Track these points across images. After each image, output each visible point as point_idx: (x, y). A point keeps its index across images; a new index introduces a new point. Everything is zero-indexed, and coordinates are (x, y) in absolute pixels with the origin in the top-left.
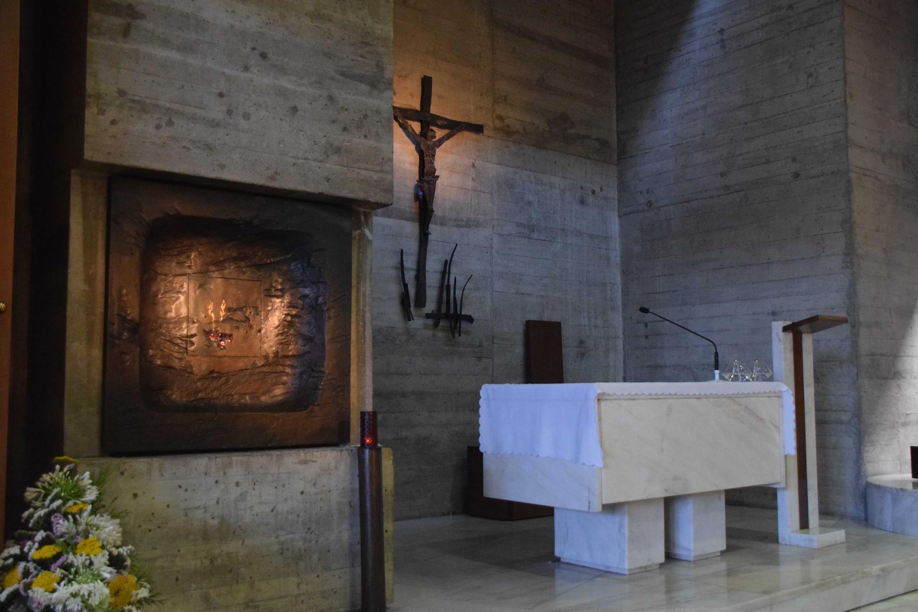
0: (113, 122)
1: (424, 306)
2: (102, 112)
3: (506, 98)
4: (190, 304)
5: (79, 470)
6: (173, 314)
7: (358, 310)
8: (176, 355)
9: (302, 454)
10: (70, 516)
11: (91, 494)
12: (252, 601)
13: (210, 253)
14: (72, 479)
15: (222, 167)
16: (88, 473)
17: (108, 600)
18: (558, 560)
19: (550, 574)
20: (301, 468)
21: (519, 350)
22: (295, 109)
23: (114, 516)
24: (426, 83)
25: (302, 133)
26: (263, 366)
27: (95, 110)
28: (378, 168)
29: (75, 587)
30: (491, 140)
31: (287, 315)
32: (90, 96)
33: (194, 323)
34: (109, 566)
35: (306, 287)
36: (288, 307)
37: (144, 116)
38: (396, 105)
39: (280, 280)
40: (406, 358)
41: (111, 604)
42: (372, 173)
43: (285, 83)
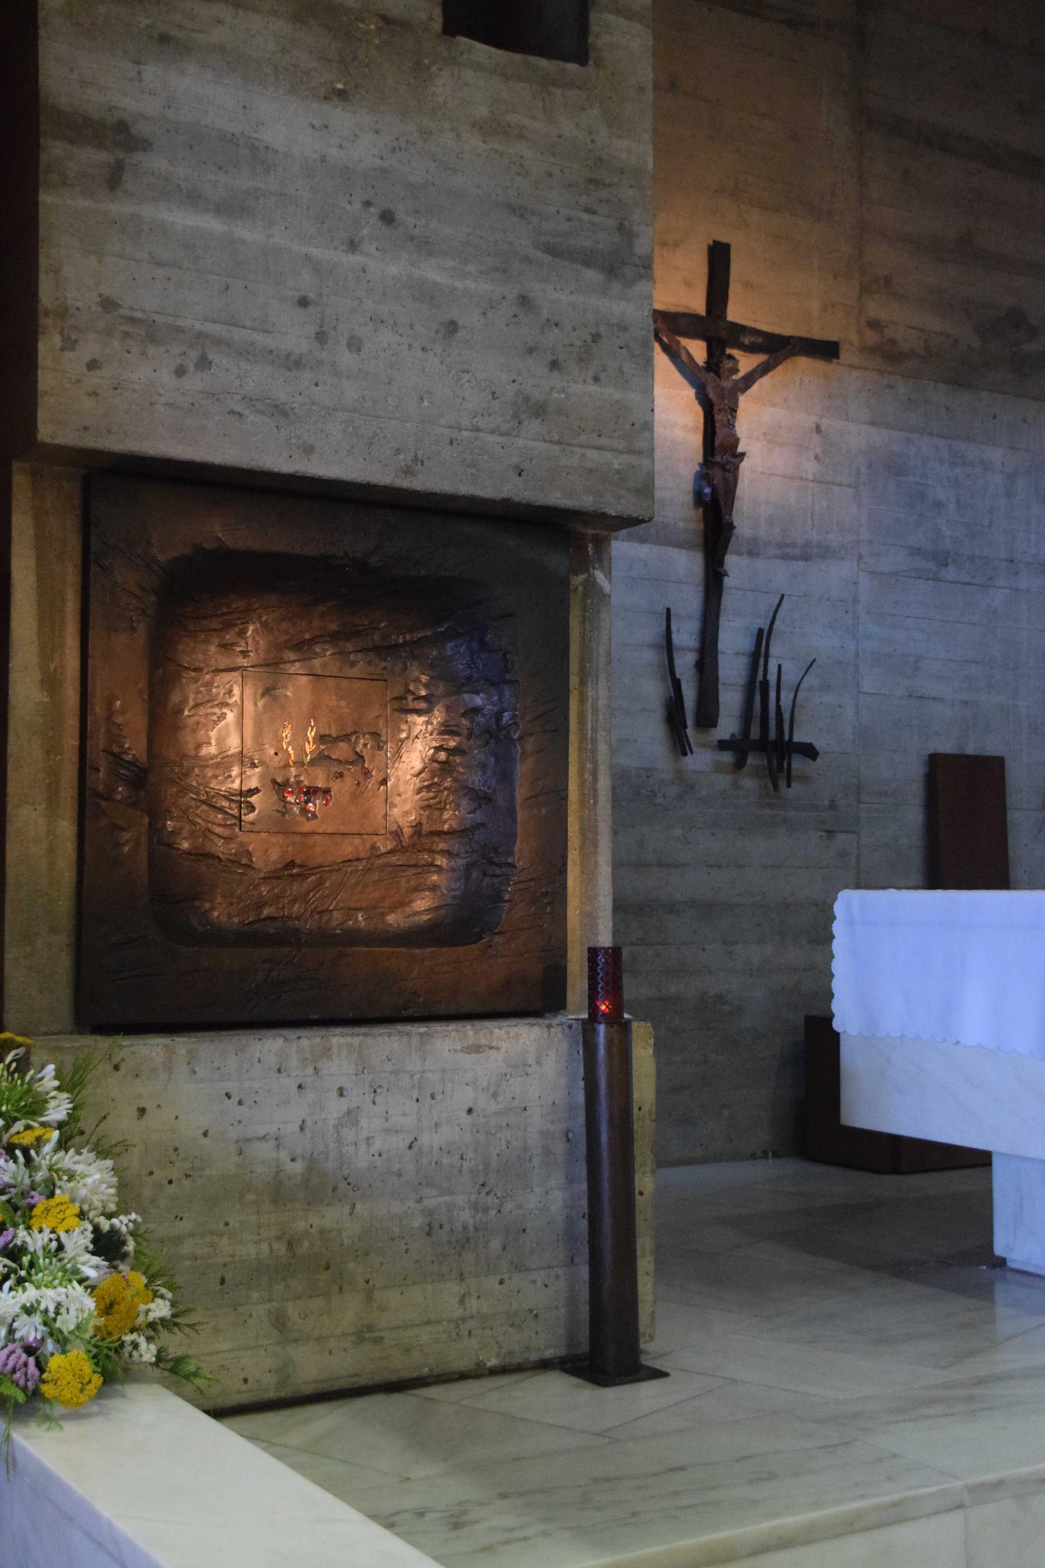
0: (93, 365)
1: (714, 725)
2: (69, 344)
3: (888, 281)
4: (245, 726)
5: (34, 1059)
6: (213, 750)
7: (583, 737)
8: (218, 830)
9: (470, 1032)
10: (18, 1152)
11: (58, 1110)
12: (370, 1328)
13: (283, 625)
14: (23, 1079)
15: (308, 450)
16: (51, 1068)
17: (92, 1323)
18: (1002, 1262)
19: (984, 1292)
20: (467, 1060)
21: (914, 816)
22: (452, 327)
23: (101, 1152)
24: (719, 257)
25: (467, 377)
26: (391, 852)
27: (57, 340)
28: (621, 445)
29: (30, 1294)
30: (855, 374)
31: (437, 749)
32: (47, 313)
33: (254, 765)
34: (93, 1253)
35: (477, 693)
36: (441, 733)
37: (151, 350)
38: (658, 306)
39: (424, 678)
40: (677, 832)
41: (97, 1329)
42: (609, 454)
43: (433, 272)
